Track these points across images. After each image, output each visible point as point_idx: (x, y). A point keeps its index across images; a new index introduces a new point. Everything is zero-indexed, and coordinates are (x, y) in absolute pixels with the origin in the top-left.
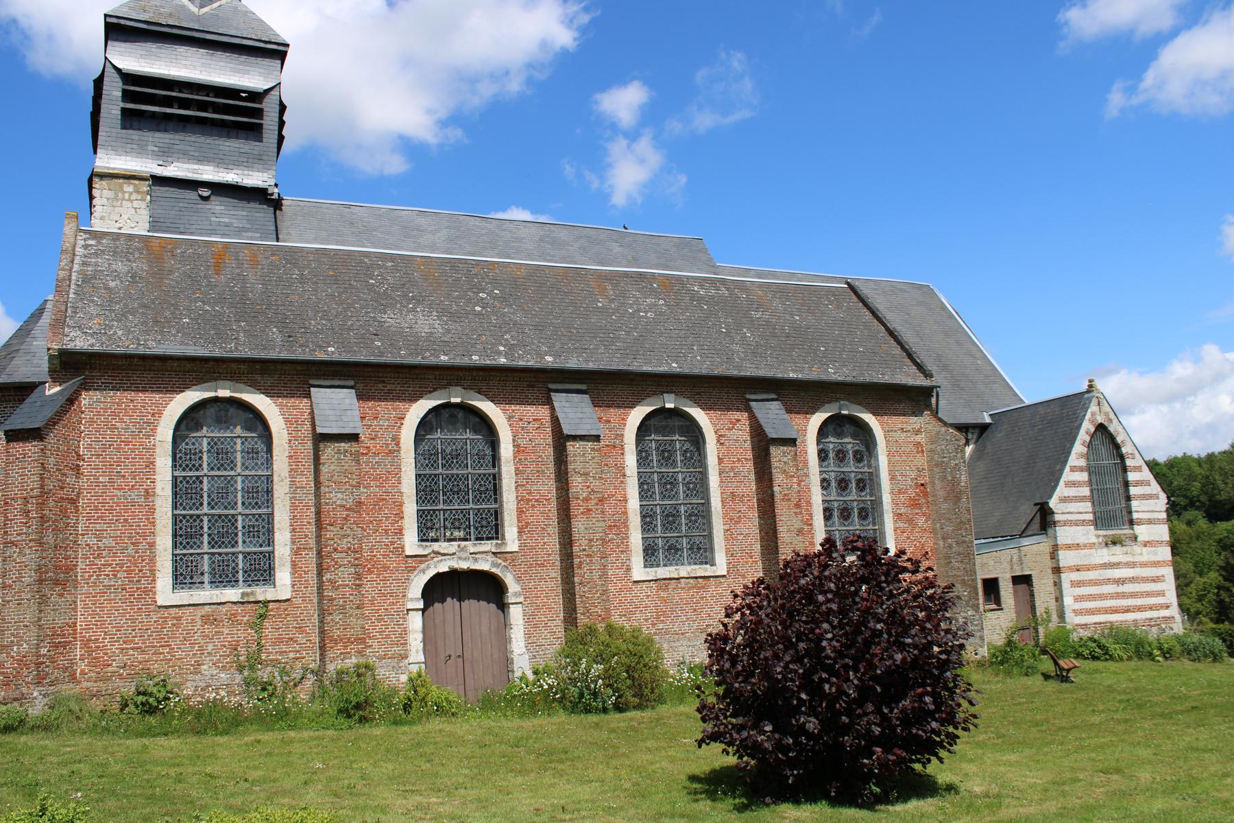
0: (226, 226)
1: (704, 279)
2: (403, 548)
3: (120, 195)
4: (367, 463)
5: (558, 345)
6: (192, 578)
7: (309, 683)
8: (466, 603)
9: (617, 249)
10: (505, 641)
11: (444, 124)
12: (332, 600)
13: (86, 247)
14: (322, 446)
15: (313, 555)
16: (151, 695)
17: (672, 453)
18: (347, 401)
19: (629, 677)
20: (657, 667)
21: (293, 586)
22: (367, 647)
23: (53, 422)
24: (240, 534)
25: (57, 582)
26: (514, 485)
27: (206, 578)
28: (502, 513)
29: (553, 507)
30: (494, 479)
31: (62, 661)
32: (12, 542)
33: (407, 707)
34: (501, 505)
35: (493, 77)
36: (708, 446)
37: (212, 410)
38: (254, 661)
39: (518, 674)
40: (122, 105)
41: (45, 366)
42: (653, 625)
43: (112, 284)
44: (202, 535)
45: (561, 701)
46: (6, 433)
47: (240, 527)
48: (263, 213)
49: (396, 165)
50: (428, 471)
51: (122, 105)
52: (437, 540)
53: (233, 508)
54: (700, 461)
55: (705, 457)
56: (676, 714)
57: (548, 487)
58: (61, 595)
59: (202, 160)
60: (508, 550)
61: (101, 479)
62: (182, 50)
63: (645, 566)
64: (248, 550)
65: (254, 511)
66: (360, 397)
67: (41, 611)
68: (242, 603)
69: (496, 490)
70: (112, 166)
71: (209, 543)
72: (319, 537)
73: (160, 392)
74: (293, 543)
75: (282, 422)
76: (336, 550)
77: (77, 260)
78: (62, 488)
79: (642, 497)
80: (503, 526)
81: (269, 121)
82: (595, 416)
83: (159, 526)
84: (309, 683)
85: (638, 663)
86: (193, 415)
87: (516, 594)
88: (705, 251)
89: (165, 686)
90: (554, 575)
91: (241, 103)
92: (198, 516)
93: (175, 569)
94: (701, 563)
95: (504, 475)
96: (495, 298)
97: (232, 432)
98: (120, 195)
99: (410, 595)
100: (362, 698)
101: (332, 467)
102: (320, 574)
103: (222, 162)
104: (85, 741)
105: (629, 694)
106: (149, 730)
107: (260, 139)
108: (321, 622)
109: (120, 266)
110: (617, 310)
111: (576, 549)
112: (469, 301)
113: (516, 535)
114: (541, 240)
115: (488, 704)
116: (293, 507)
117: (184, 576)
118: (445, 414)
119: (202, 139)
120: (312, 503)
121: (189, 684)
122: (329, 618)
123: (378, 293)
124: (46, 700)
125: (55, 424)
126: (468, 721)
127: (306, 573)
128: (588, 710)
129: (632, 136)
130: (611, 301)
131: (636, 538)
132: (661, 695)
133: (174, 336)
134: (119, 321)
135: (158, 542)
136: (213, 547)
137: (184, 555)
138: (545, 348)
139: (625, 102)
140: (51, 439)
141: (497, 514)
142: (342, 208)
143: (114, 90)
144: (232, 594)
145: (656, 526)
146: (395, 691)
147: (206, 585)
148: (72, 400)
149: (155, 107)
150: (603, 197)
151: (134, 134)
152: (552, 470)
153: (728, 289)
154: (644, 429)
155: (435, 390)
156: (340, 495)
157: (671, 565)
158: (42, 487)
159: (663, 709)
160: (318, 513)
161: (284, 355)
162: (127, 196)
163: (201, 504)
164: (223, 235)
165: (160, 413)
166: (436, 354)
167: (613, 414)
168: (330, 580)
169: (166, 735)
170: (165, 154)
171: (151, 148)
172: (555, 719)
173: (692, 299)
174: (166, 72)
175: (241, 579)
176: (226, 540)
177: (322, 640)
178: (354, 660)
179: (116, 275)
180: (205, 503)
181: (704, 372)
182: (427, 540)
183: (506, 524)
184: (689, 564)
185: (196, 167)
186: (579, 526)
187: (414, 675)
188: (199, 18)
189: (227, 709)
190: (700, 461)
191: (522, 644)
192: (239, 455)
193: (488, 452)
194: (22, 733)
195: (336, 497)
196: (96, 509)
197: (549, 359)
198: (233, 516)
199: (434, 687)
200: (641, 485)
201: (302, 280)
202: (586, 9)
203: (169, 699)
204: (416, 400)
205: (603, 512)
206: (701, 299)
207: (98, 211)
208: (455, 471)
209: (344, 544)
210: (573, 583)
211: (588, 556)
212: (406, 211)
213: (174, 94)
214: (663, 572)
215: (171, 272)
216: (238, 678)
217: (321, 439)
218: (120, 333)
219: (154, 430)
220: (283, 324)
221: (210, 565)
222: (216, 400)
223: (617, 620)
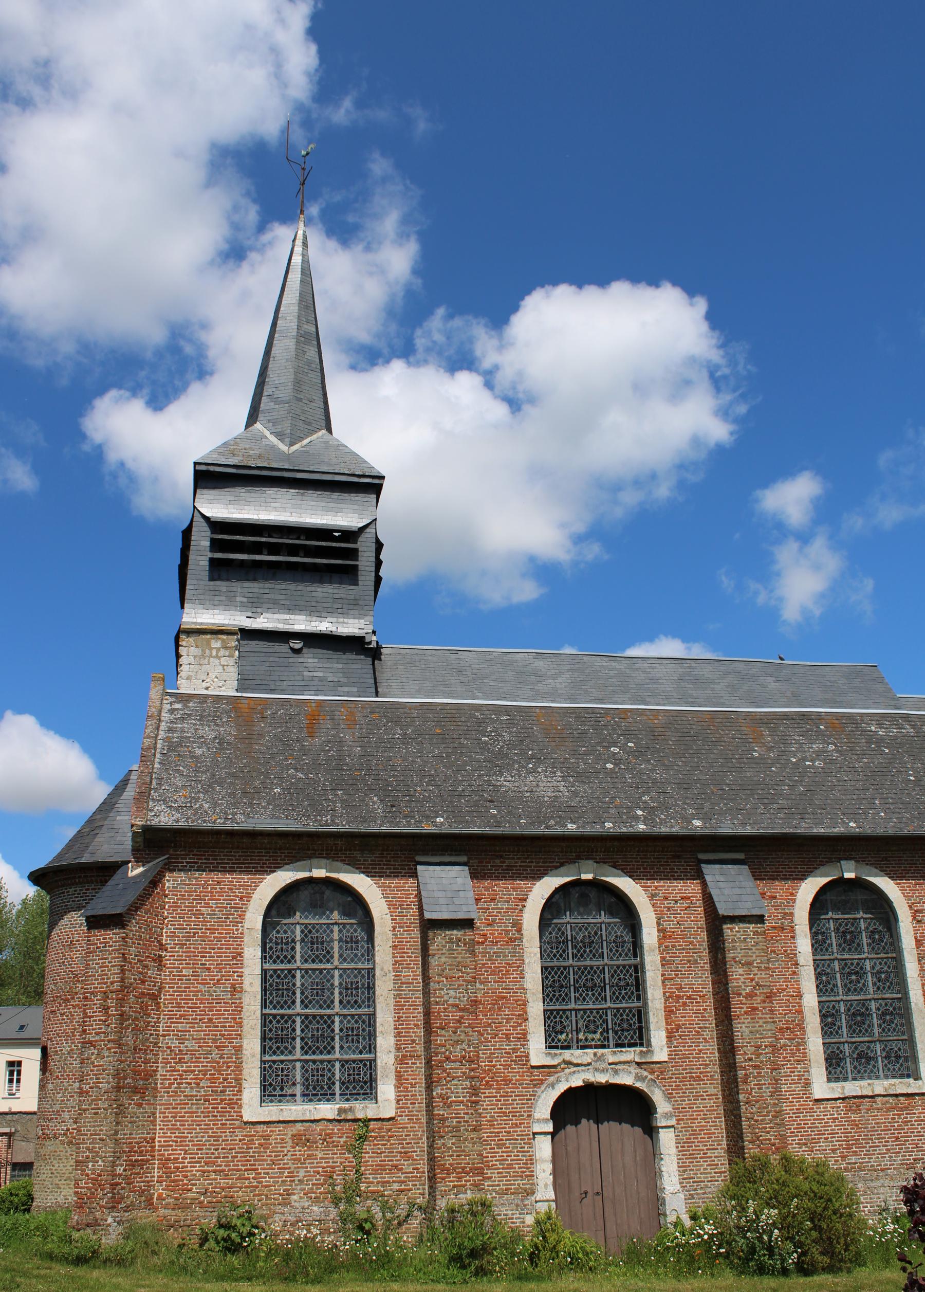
0: (321, 684)
1: (883, 716)
2: (527, 1056)
3: (207, 651)
4: (484, 954)
5: (707, 806)
6: (282, 1089)
7: (415, 1223)
8: (605, 1126)
9: (772, 685)
10: (654, 1175)
11: (579, 539)
12: (444, 1120)
13: (172, 711)
14: (431, 934)
15: (420, 1064)
16: (233, 1228)
17: (856, 934)
18: (460, 880)
19: (815, 1227)
20: (850, 1215)
21: (398, 1102)
22: (484, 1179)
23: (135, 907)
24: (337, 1038)
25: (135, 1090)
26: (660, 978)
27: (298, 1090)
28: (647, 1013)
29: (709, 1004)
30: (636, 971)
31: (139, 1184)
32: (90, 1042)
33: (533, 1258)
34: (646, 1004)
35: (637, 483)
36: (901, 924)
37: (306, 893)
38: (352, 1193)
39: (671, 1218)
40: (210, 555)
41: (129, 844)
42: (844, 1157)
43: (199, 752)
44: (294, 1039)
45: (727, 1256)
46: (88, 919)
47: (337, 1030)
48: (359, 664)
49: (528, 591)
50: (555, 963)
51: (210, 555)
52: (568, 1047)
53: (328, 1007)
54: (892, 944)
55: (898, 939)
56: (881, 1282)
57: (701, 980)
58: (140, 1105)
59: (293, 609)
60: (655, 1059)
61: (184, 972)
62: (271, 492)
63: (829, 1080)
64: (346, 1057)
65: (353, 1011)
66: (474, 875)
67: (118, 1123)
68: (339, 1121)
69: (639, 985)
70: (199, 621)
71: (302, 1048)
72: (428, 1042)
73: (248, 872)
74: (398, 1049)
75: (384, 906)
76: (448, 1058)
77: (163, 726)
78: (143, 982)
79: (820, 991)
80: (648, 1029)
81: (365, 562)
82: (756, 891)
83: (246, 1028)
84: (415, 1223)
85: (825, 1208)
86: (283, 898)
87: (667, 1116)
88: (882, 680)
89: (250, 1219)
90: (714, 1091)
91: (334, 544)
92: (290, 1016)
93: (264, 1078)
94: (902, 1076)
95: (648, 967)
96: (629, 752)
97: (328, 918)
98: (207, 651)
99: (537, 1115)
100: (479, 1243)
101: (443, 959)
102: (429, 1088)
103: (315, 610)
104: (160, 1282)
105: (815, 1251)
106: (231, 1272)
107: (356, 583)
108: (431, 1146)
109: (207, 732)
110: (776, 760)
111: (739, 1058)
112: (598, 758)
113: (664, 1040)
114: (681, 679)
115: (634, 1257)
116: (398, 1007)
117: (273, 1088)
118: (575, 893)
119: (293, 586)
120: (419, 1002)
121: (277, 1217)
122: (440, 1142)
123: (493, 752)
124: (120, 1228)
125: (137, 909)
126: (609, 1279)
127: (413, 1086)
128: (762, 1270)
129: (804, 538)
130: (770, 749)
131: (815, 1044)
132: (858, 1254)
133: (265, 808)
134: (206, 792)
135: (245, 1046)
136: (306, 1053)
137: (274, 1062)
138: (691, 811)
139: (793, 497)
140: (133, 926)
141: (641, 1015)
142: (448, 654)
143: (202, 539)
144: (327, 1110)
145: (840, 1028)
146: (517, 1237)
147: (298, 1098)
148: (155, 882)
149: (243, 555)
150: (772, 614)
151: (222, 585)
152: (707, 959)
153: (913, 727)
154: (818, 905)
155: (562, 865)
156: (452, 993)
157: (862, 1078)
158: (122, 980)
159: (862, 1274)
160: (427, 1014)
161: (386, 828)
162: (214, 653)
163: (294, 1002)
164: (318, 692)
165: (249, 897)
166: (562, 823)
167: (779, 888)
168: (441, 1096)
169: (250, 1279)
170: (254, 606)
171: (239, 599)
172: (720, 1282)
173: (869, 741)
174: (256, 517)
175: (338, 1091)
176: (321, 1045)
177: (432, 1169)
178: (469, 1195)
179: (203, 742)
180: (298, 1001)
181: (891, 832)
182: (556, 1047)
183: (652, 1027)
184: (886, 1077)
185: (287, 617)
186: (742, 1029)
187: (542, 1216)
188: (288, 457)
189: (318, 1251)
190: (892, 944)
191: (676, 1179)
192: (336, 945)
193: (628, 938)
194: (94, 1267)
195: (448, 995)
196: (179, 1006)
197: (697, 823)
198: (329, 1016)
199: (567, 1233)
200: (818, 975)
201: (405, 740)
202: (743, 397)
203: (254, 1235)
204: (540, 878)
205: (772, 1011)
206: (880, 741)
207: (185, 670)
208: (588, 963)
209: (458, 1052)
210: (738, 1102)
211: (756, 1067)
212: (522, 653)
213: (263, 539)
214: (852, 1088)
215: (261, 736)
216: (333, 1213)
217: (429, 926)
218: (206, 806)
219: (242, 916)
220: (384, 793)
221: (303, 1076)
222: (310, 881)
223: (795, 1150)
